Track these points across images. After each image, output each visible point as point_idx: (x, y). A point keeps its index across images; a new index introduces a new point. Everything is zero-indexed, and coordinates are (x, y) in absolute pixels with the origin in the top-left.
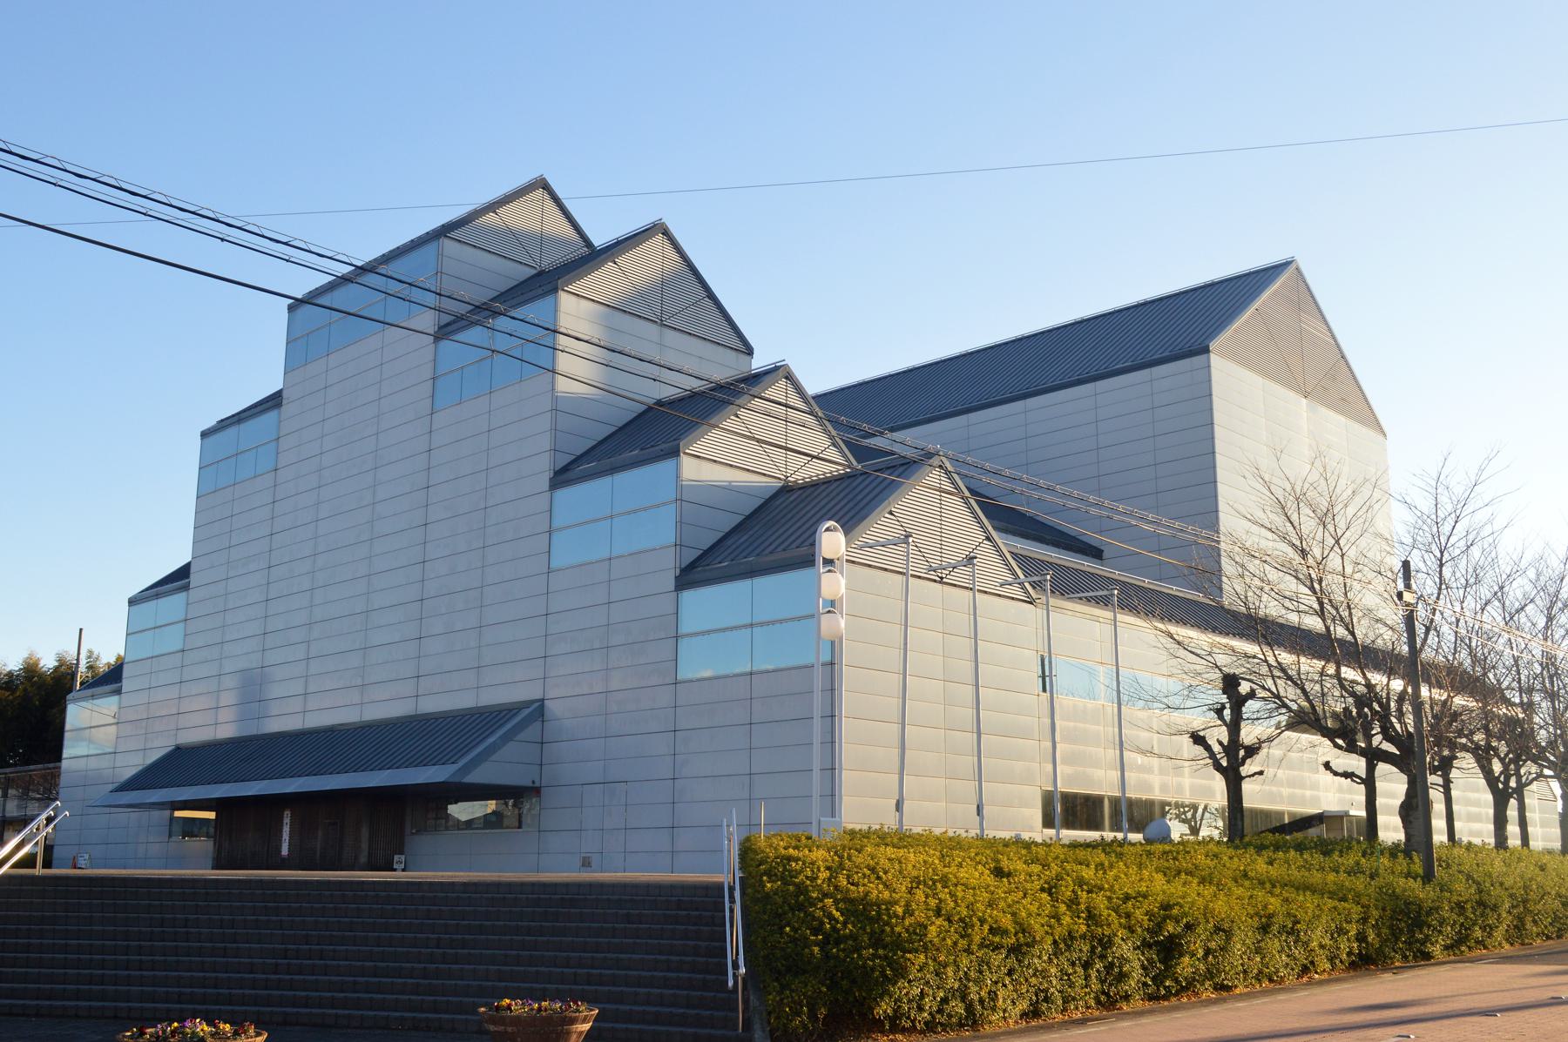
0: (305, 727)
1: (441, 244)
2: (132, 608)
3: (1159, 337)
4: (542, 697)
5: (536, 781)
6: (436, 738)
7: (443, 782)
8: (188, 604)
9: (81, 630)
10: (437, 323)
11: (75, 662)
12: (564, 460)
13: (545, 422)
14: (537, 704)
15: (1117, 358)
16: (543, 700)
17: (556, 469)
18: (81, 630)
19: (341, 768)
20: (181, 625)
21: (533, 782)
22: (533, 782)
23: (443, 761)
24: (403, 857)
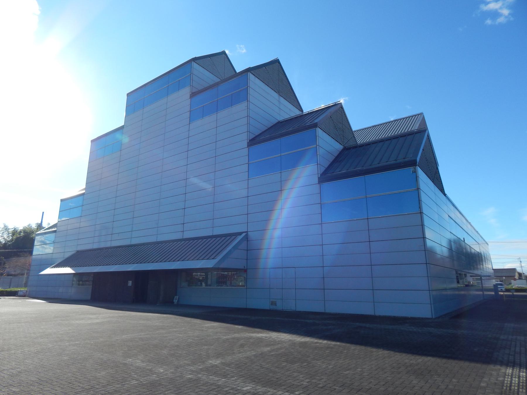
0: (132, 244)
1: (192, 64)
2: (62, 202)
3: (124, 256)
4: (247, 231)
5: (245, 267)
6: (139, 259)
7: (212, 268)
8: (83, 200)
9: (43, 212)
10: (191, 91)
11: (175, 301)
12: (253, 136)
13: (245, 121)
14: (244, 234)
15: (112, 261)
16: (247, 232)
17: (250, 139)
18: (43, 212)
19: (124, 262)
20: (81, 208)
21: (244, 267)
22: (244, 267)
23: (133, 263)
24: (178, 297)
